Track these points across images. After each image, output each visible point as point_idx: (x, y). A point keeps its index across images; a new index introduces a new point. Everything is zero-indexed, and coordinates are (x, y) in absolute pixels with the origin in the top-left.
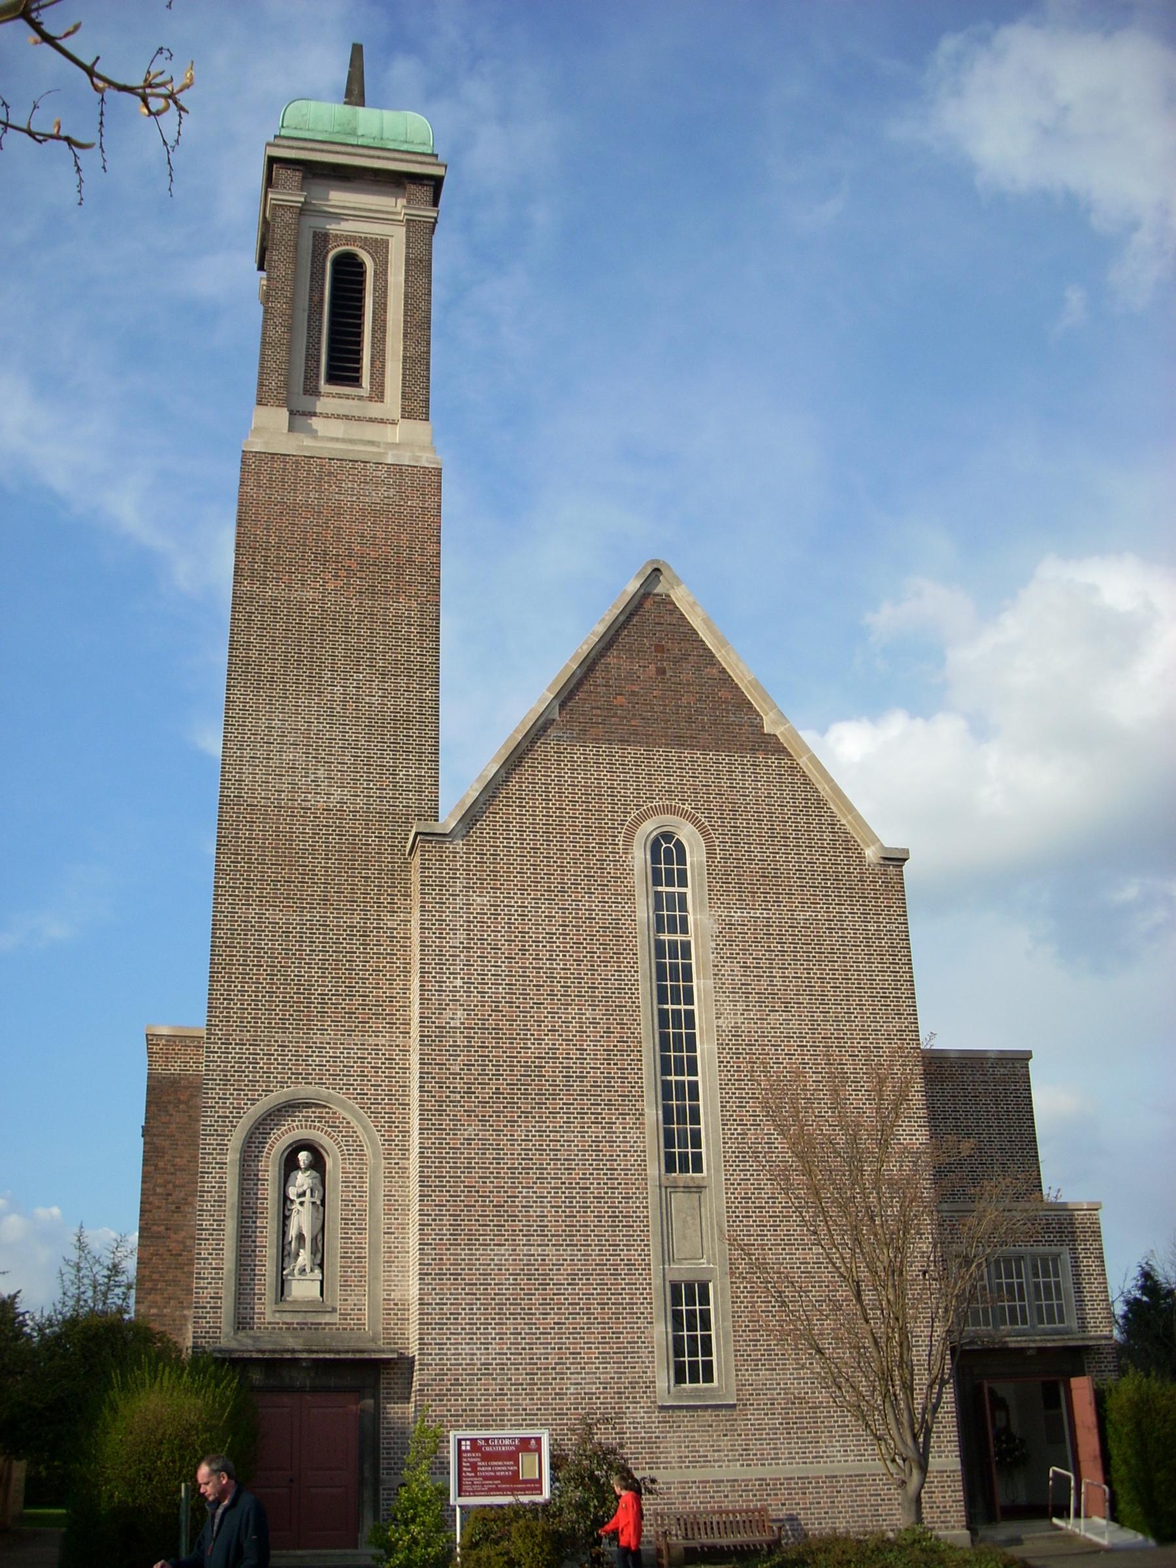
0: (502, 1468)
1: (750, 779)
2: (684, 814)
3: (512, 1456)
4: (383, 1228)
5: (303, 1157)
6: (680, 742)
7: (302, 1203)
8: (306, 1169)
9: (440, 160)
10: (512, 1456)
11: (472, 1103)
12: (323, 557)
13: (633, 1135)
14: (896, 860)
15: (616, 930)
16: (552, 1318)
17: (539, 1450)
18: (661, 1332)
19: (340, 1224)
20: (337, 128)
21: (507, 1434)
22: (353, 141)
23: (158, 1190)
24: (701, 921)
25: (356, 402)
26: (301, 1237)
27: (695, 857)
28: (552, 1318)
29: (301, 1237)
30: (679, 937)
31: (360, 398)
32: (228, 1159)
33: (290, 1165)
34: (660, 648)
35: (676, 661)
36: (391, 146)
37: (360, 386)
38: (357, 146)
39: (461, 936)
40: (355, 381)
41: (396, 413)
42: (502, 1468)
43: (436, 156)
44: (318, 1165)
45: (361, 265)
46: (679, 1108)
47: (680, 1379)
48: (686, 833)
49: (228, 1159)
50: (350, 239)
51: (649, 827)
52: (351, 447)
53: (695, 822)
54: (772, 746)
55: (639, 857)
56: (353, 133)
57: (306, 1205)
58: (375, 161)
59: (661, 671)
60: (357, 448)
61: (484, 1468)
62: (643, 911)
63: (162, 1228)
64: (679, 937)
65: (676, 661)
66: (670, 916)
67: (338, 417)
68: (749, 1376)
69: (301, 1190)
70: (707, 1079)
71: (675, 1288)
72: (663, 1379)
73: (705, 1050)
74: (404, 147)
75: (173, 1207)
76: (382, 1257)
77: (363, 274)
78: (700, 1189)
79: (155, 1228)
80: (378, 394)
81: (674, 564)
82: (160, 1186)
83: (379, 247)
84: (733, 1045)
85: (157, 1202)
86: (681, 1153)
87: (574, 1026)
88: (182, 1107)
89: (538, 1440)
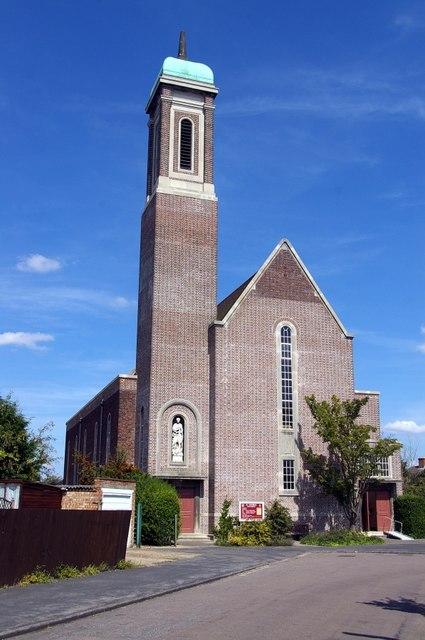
0: (252, 512)
5: (178, 419)
6: (290, 298)
10: (255, 509)
12: (182, 230)
15: (271, 357)
18: (281, 474)
21: (253, 503)
24: (295, 355)
27: (294, 334)
30: (284, 358)
33: (175, 421)
35: (289, 272)
40: (189, 167)
42: (252, 512)
44: (182, 422)
45: (191, 124)
48: (291, 326)
51: (281, 325)
55: (278, 334)
61: (248, 512)
62: (279, 351)
64: (288, 359)
65: (289, 272)
66: (286, 353)
71: (285, 461)
72: (281, 488)
73: (295, 392)
74: (204, 80)
80: (196, 173)
81: (336, 393)
83: (196, 117)
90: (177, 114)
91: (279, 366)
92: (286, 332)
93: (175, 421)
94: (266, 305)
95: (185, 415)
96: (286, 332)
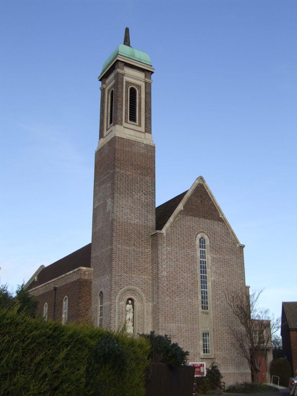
1: (217, 227)
2: (205, 233)
3: (199, 367)
4: (146, 318)
7: (130, 312)
8: (130, 305)
9: (153, 67)
10: (199, 367)
11: (168, 293)
13: (196, 301)
14: (242, 247)
16: (182, 339)
17: (204, 366)
19: (137, 317)
20: (131, 55)
22: (134, 58)
23: (83, 306)
25: (135, 126)
26: (129, 319)
27: (207, 243)
28: (182, 339)
29: (129, 319)
31: (136, 125)
32: (116, 301)
34: (201, 196)
36: (142, 61)
37: (136, 122)
38: (135, 60)
39: (166, 256)
41: (144, 131)
43: (152, 66)
44: (133, 304)
46: (204, 297)
47: (204, 353)
48: (206, 237)
49: (116, 301)
50: (133, 84)
51: (199, 236)
52: (130, 137)
53: (207, 235)
54: (222, 221)
55: (198, 242)
56: (134, 56)
57: (131, 312)
58: (138, 65)
59: (201, 201)
60: (138, 139)
63: (84, 315)
67: (132, 129)
68: (216, 352)
69: (130, 309)
70: (209, 290)
71: (203, 334)
72: (202, 353)
73: (209, 284)
75: (86, 309)
76: (146, 324)
77: (135, 93)
78: (208, 313)
79: (82, 314)
80: (140, 125)
82: (83, 305)
84: (214, 283)
85: (83, 308)
86: (205, 308)
87: (186, 278)
88: (88, 286)
89: (204, 364)
90: (128, 83)
91: (199, 265)
92: (202, 241)
93: (127, 303)
94: (190, 221)
95: (134, 298)
96: (202, 241)
